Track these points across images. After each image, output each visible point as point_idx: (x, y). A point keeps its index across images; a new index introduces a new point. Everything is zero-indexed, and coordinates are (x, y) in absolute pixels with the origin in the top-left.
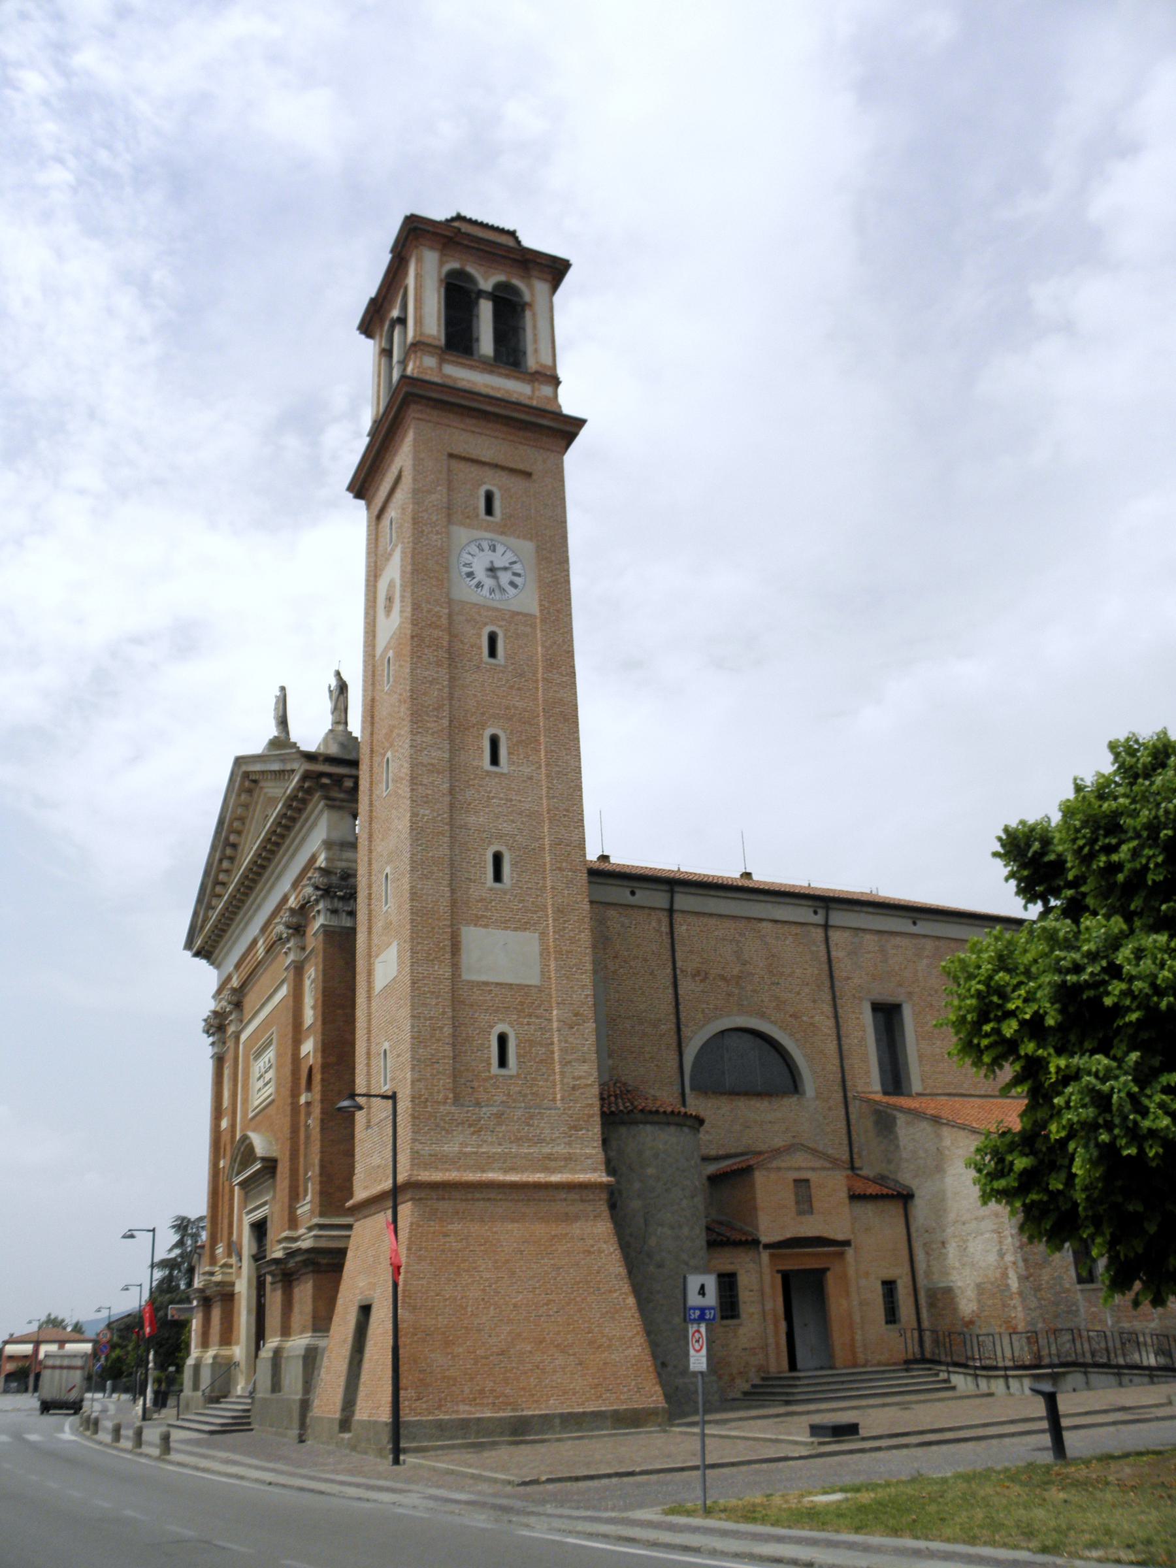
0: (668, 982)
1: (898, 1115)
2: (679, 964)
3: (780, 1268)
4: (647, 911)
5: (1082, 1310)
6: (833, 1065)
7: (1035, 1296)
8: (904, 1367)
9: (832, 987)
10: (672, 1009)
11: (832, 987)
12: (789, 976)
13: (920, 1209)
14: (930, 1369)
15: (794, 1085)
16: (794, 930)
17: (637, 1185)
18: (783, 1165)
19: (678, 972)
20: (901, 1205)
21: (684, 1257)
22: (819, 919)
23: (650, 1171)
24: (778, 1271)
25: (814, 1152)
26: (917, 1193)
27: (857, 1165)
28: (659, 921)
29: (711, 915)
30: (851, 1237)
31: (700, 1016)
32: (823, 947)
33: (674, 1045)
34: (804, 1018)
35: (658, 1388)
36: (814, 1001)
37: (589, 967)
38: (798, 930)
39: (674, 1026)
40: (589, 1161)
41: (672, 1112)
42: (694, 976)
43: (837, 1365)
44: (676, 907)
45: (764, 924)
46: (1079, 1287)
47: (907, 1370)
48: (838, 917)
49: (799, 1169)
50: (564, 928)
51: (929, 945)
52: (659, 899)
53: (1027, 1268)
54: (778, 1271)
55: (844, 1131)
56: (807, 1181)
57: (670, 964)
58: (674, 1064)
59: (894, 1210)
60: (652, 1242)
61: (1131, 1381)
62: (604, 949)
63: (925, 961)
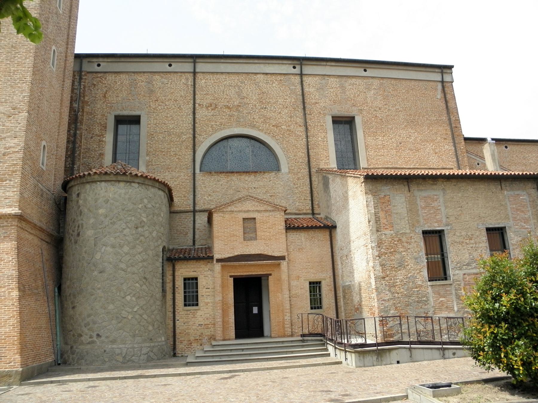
0: (190, 112)
1: (330, 176)
2: (198, 101)
3: (233, 274)
4: (179, 74)
5: (431, 299)
6: (302, 154)
7: (390, 291)
8: (300, 338)
9: (304, 108)
10: (191, 126)
11: (304, 108)
12: (274, 103)
13: (339, 233)
14: (322, 340)
15: (278, 169)
16: (279, 78)
17: (92, 221)
18: (235, 209)
19: (197, 105)
20: (328, 233)
21: (123, 266)
22: (297, 71)
23: (101, 211)
24: (231, 276)
25: (260, 201)
26: (339, 225)
27: (316, 212)
28: (187, 79)
29: (222, 73)
30: (286, 254)
31: (210, 129)
32: (299, 87)
33: (191, 146)
34: (283, 127)
35: (18, 357)
36: (291, 117)
37: (29, 79)
38: (282, 78)
39: (191, 136)
40: (7, 201)
41: (142, 176)
42: (207, 107)
43: (273, 335)
44: (197, 70)
45: (258, 76)
46: (429, 283)
47: (303, 341)
48: (308, 69)
49: (248, 211)
50: (15, 57)
51: (376, 82)
52: (188, 67)
53: (383, 271)
54: (231, 276)
55: (309, 191)
56: (254, 219)
57: (192, 102)
58: (191, 158)
59: (323, 236)
60: (98, 256)
61: (454, 354)
62: (150, 97)
63: (372, 92)
